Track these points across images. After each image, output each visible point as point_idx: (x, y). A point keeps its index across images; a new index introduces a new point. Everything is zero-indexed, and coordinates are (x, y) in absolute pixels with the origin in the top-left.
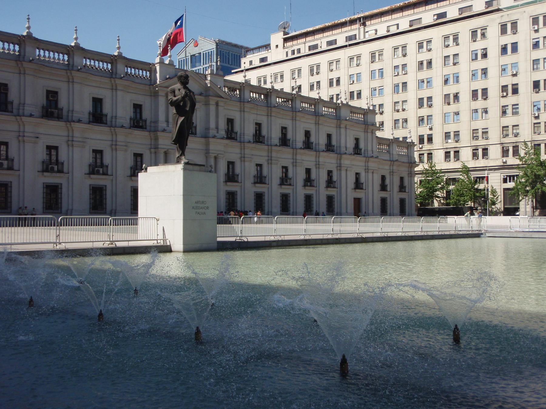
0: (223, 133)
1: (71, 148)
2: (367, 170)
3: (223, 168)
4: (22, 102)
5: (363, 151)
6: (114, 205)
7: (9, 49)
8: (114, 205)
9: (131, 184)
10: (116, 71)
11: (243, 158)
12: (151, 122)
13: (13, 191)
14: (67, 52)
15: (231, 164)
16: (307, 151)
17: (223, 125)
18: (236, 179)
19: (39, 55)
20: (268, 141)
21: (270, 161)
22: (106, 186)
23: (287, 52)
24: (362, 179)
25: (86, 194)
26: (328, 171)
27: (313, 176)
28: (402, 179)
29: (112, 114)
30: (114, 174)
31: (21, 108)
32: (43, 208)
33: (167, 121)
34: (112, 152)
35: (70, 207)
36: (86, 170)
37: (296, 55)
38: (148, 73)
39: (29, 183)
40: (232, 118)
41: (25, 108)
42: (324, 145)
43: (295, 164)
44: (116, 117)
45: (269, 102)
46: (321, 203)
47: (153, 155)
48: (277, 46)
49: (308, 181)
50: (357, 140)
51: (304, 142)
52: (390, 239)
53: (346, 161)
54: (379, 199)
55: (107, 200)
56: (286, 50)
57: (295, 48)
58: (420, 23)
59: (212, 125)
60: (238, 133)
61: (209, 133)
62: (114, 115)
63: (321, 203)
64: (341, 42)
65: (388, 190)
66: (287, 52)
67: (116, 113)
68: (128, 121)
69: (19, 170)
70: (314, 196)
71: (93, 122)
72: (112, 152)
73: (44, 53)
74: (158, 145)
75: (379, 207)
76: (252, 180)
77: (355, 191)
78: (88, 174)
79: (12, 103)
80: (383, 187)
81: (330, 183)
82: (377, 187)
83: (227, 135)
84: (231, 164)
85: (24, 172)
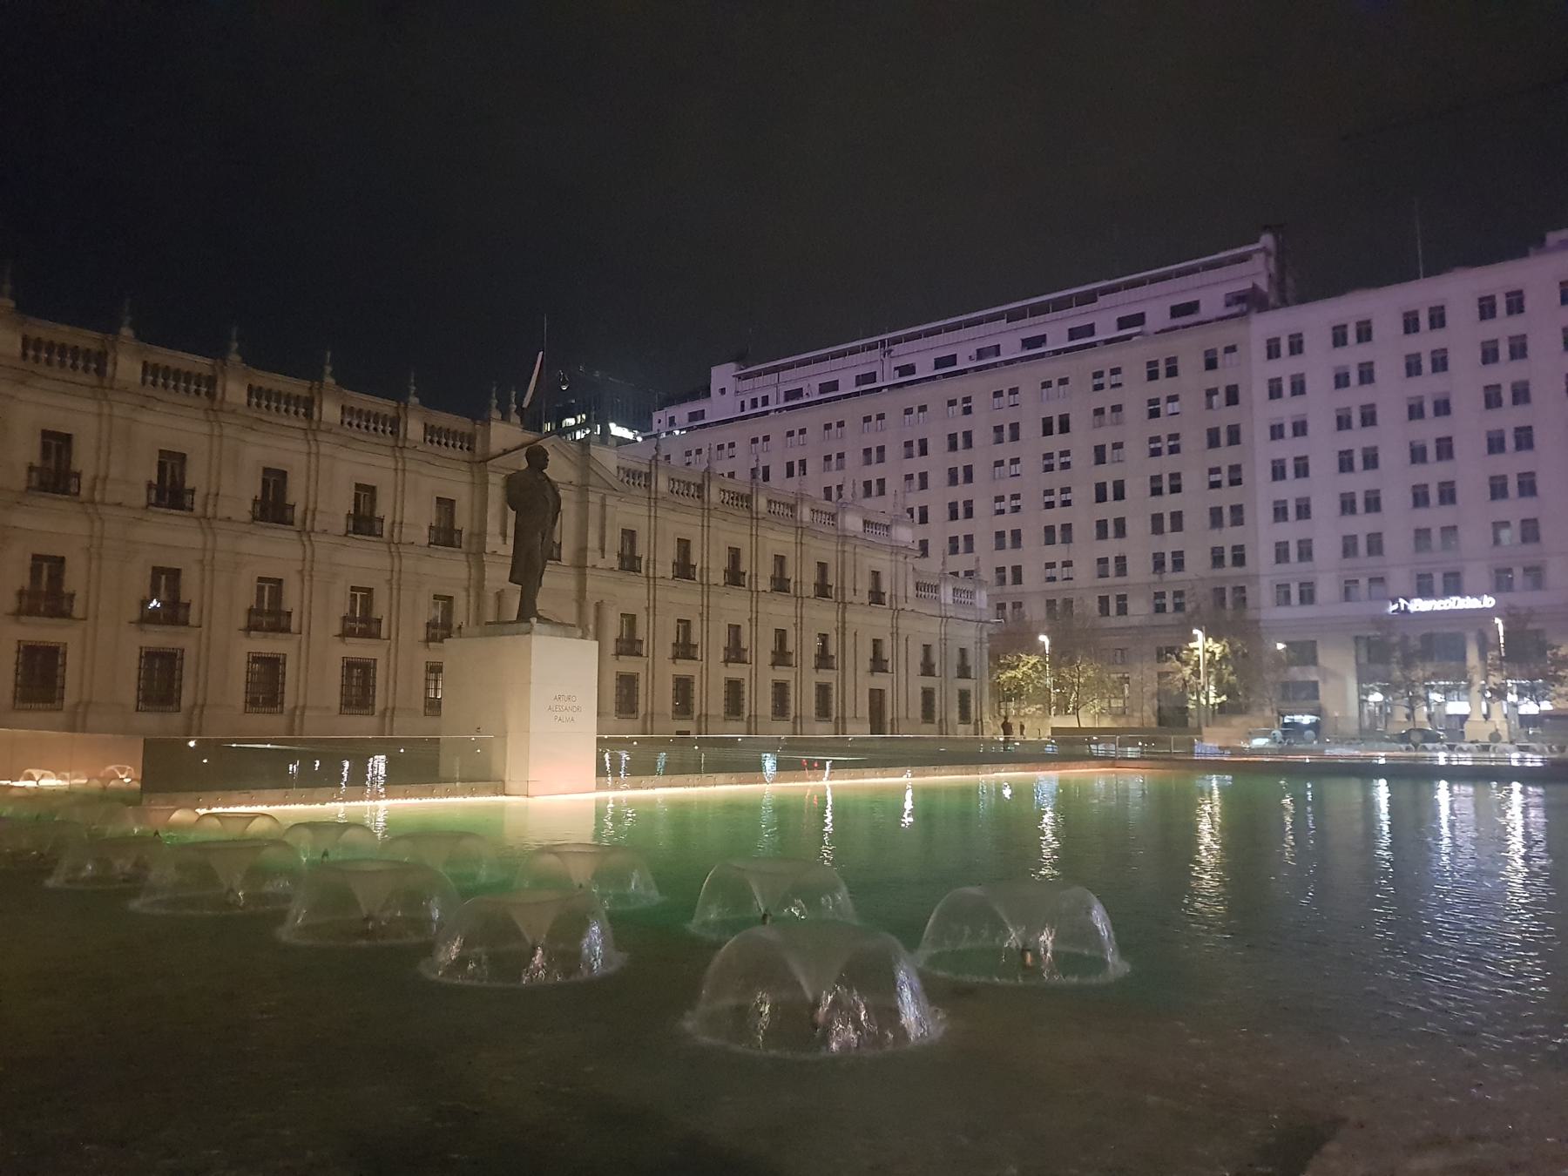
0: (613, 560)
2: (895, 634)
3: (613, 629)
15: (630, 620)
16: (778, 596)
17: (614, 541)
18: (66, 607)
20: (205, 506)
21: (705, 615)
24: (887, 653)
31: (99, 486)
33: (603, 550)
37: (760, 409)
43: (799, 625)
48: (723, 391)
49: (684, 649)
50: (822, 567)
51: (773, 579)
53: (855, 618)
56: (742, 398)
57: (759, 396)
58: (998, 354)
64: (847, 386)
70: (792, 684)
71: (157, 505)
76: (670, 652)
77: (248, 636)
79: (78, 475)
80: (928, 669)
81: (824, 660)
83: (622, 563)
84: (630, 620)
85: (209, 628)
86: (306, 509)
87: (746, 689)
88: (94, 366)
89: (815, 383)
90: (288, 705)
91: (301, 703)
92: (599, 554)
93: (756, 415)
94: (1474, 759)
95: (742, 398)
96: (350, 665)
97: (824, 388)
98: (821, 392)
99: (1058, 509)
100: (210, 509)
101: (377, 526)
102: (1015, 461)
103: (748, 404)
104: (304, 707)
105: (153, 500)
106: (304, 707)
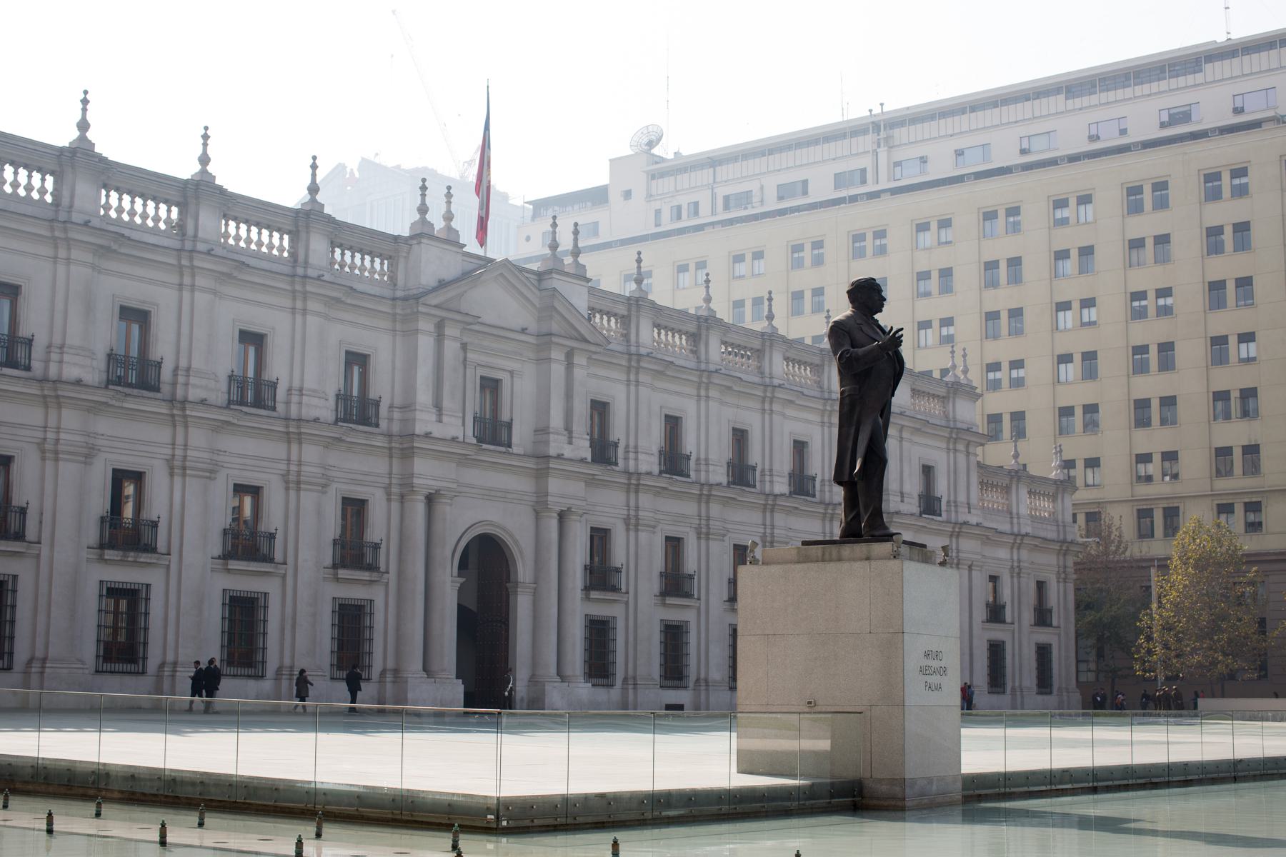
0: (582, 448)
1: (178, 480)
2: (403, 491)
4: (57, 340)
5: (166, 374)
6: (287, 653)
7: (29, 188)
8: (287, 653)
9: (729, 619)
10: (307, 256)
11: (633, 523)
12: (391, 407)
13: (19, 604)
14: (181, 200)
16: (798, 502)
19: (15, 185)
22: (15, 577)
23: (658, 212)
25: (214, 615)
26: (115, 470)
27: (618, 556)
28: (1041, 585)
29: (392, 399)
30: (703, 597)
31: (54, 357)
32: (98, 656)
33: (438, 406)
34: (287, 495)
35: (170, 657)
36: (92, 534)
38: (175, 210)
39: (61, 581)
40: (604, 399)
41: (66, 358)
42: (786, 474)
44: (188, 369)
45: (703, 357)
46: (638, 649)
47: (395, 506)
50: (927, 471)
51: (343, 398)
52: (69, 785)
54: (1034, 649)
55: (269, 636)
57: (684, 200)
59: (556, 420)
60: (693, 458)
61: (547, 443)
62: (296, 384)
63: (638, 649)
65: (1008, 619)
66: (658, 212)
67: (302, 380)
68: (223, 386)
69: (169, 554)
70: (620, 625)
72: (287, 495)
73: (16, 173)
74: (412, 475)
75: (1034, 673)
77: (101, 559)
78: (219, 558)
82: (1028, 616)
85: (52, 545)
86: (176, 369)
87: (693, 638)
88: (337, 267)
89: (771, 184)
90: (152, 664)
91: (170, 658)
92: (564, 439)
93: (681, 231)
94: (747, 763)
95: (657, 205)
96: (113, 592)
97: (784, 192)
98: (780, 198)
99: (935, 318)
100: (632, 463)
101: (372, 411)
102: (1088, 303)
103: (666, 215)
104: (44, 660)
105: (341, 415)
106: (175, 664)
